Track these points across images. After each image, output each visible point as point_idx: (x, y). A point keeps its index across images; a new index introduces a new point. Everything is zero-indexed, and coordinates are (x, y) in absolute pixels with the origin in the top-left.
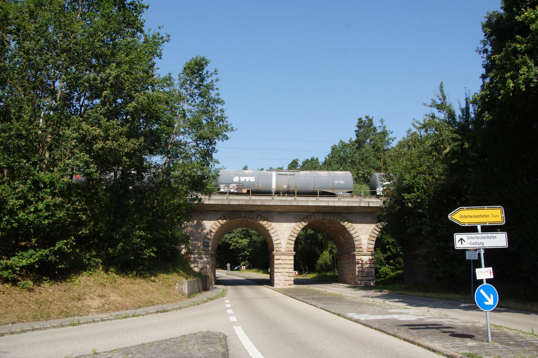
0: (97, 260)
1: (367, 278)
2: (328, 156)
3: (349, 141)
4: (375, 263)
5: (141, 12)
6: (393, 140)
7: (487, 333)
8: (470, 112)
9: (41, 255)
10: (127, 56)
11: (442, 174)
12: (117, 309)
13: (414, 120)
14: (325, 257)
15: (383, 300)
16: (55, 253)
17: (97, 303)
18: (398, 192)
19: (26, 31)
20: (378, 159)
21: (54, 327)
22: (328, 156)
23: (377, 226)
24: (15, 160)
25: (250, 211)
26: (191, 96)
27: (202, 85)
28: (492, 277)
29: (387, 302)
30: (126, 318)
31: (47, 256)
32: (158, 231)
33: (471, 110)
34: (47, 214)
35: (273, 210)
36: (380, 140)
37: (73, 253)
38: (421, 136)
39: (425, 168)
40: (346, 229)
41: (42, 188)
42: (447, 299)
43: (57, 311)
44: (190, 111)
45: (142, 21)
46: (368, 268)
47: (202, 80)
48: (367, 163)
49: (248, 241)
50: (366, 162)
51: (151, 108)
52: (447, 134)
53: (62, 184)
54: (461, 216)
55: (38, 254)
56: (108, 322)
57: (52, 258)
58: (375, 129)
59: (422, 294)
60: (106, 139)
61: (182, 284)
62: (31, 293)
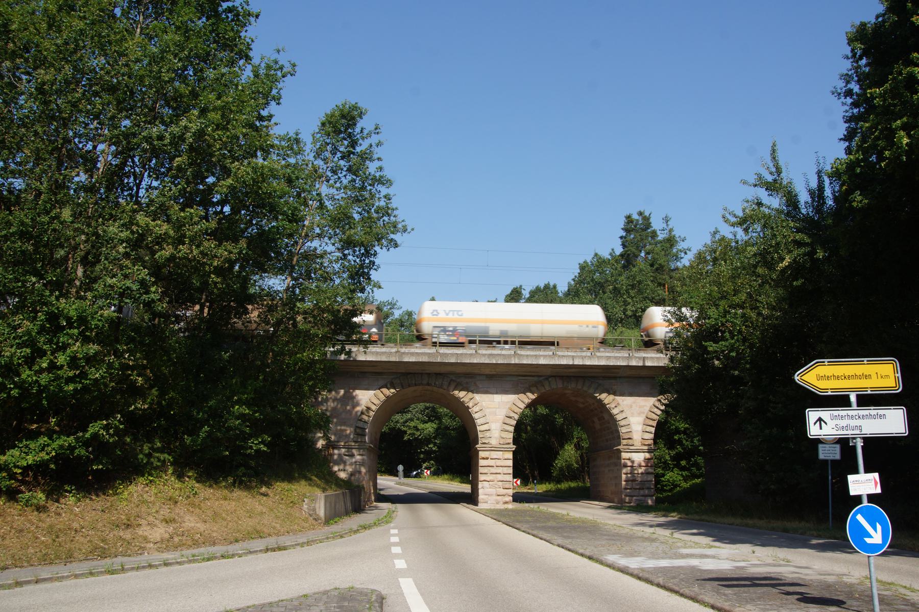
0: (164, 456)
1: (642, 492)
2: (574, 280)
3: (611, 254)
4: (655, 466)
5: (245, 25)
6: (686, 253)
7: (872, 597)
8: (826, 194)
9: (61, 447)
10: (219, 98)
11: (773, 308)
12: (196, 544)
13: (725, 209)
14: (569, 454)
15: (670, 531)
16: (86, 444)
17: (159, 532)
18: (695, 341)
19: (40, 51)
20: (660, 284)
21: (76, 576)
22: (574, 280)
23: (659, 400)
24: (15, 278)
25: (437, 374)
26: (334, 172)
27: (353, 153)
28: (878, 490)
29: (677, 535)
30: (209, 560)
31: (72, 448)
32: (273, 408)
33: (828, 192)
34: (71, 374)
35: (476, 371)
36: (663, 253)
37: (121, 444)
38: (737, 242)
39: (743, 298)
40: (604, 405)
41: (63, 328)
42: (785, 530)
43: (86, 548)
44: (332, 198)
45: (248, 40)
46: (642, 473)
47: (354, 144)
48: (640, 292)
49: (435, 426)
50: (639, 290)
51: (260, 188)
52: (788, 232)
53: (99, 320)
54: (819, 376)
55: (55, 445)
56: (177, 567)
57: (81, 452)
58: (654, 234)
59: (738, 521)
60: (180, 241)
61: (315, 499)
62: (41, 514)
